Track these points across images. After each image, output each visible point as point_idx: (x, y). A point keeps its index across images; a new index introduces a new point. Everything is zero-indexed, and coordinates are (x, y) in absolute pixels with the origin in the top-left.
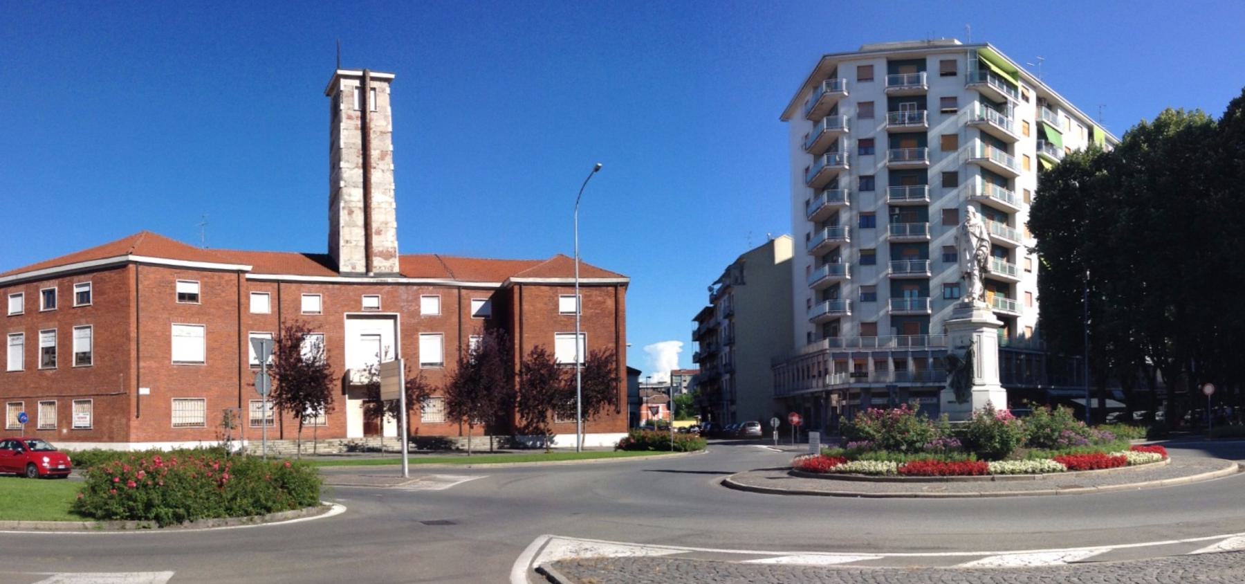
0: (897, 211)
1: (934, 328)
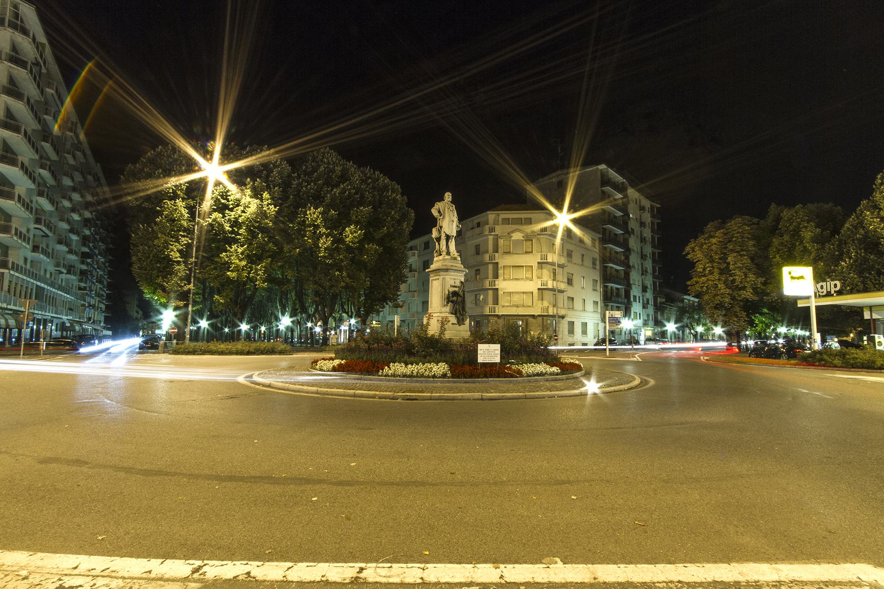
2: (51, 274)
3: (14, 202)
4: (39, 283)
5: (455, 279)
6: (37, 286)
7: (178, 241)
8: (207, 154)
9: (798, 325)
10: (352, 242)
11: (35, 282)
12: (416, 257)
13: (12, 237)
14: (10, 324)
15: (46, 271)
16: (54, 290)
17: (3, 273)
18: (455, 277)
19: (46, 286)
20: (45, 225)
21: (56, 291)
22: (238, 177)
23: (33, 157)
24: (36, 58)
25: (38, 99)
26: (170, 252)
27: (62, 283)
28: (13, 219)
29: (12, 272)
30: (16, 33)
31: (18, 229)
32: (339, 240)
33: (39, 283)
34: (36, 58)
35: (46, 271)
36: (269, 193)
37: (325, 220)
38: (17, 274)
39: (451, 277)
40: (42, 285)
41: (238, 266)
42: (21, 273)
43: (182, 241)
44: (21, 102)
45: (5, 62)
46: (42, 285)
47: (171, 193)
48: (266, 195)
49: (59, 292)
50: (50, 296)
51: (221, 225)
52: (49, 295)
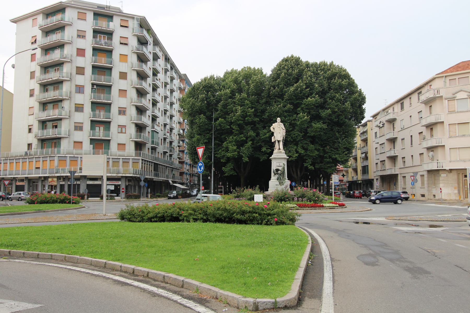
0: (95, 87)
1: (113, 147)
5: (279, 163)
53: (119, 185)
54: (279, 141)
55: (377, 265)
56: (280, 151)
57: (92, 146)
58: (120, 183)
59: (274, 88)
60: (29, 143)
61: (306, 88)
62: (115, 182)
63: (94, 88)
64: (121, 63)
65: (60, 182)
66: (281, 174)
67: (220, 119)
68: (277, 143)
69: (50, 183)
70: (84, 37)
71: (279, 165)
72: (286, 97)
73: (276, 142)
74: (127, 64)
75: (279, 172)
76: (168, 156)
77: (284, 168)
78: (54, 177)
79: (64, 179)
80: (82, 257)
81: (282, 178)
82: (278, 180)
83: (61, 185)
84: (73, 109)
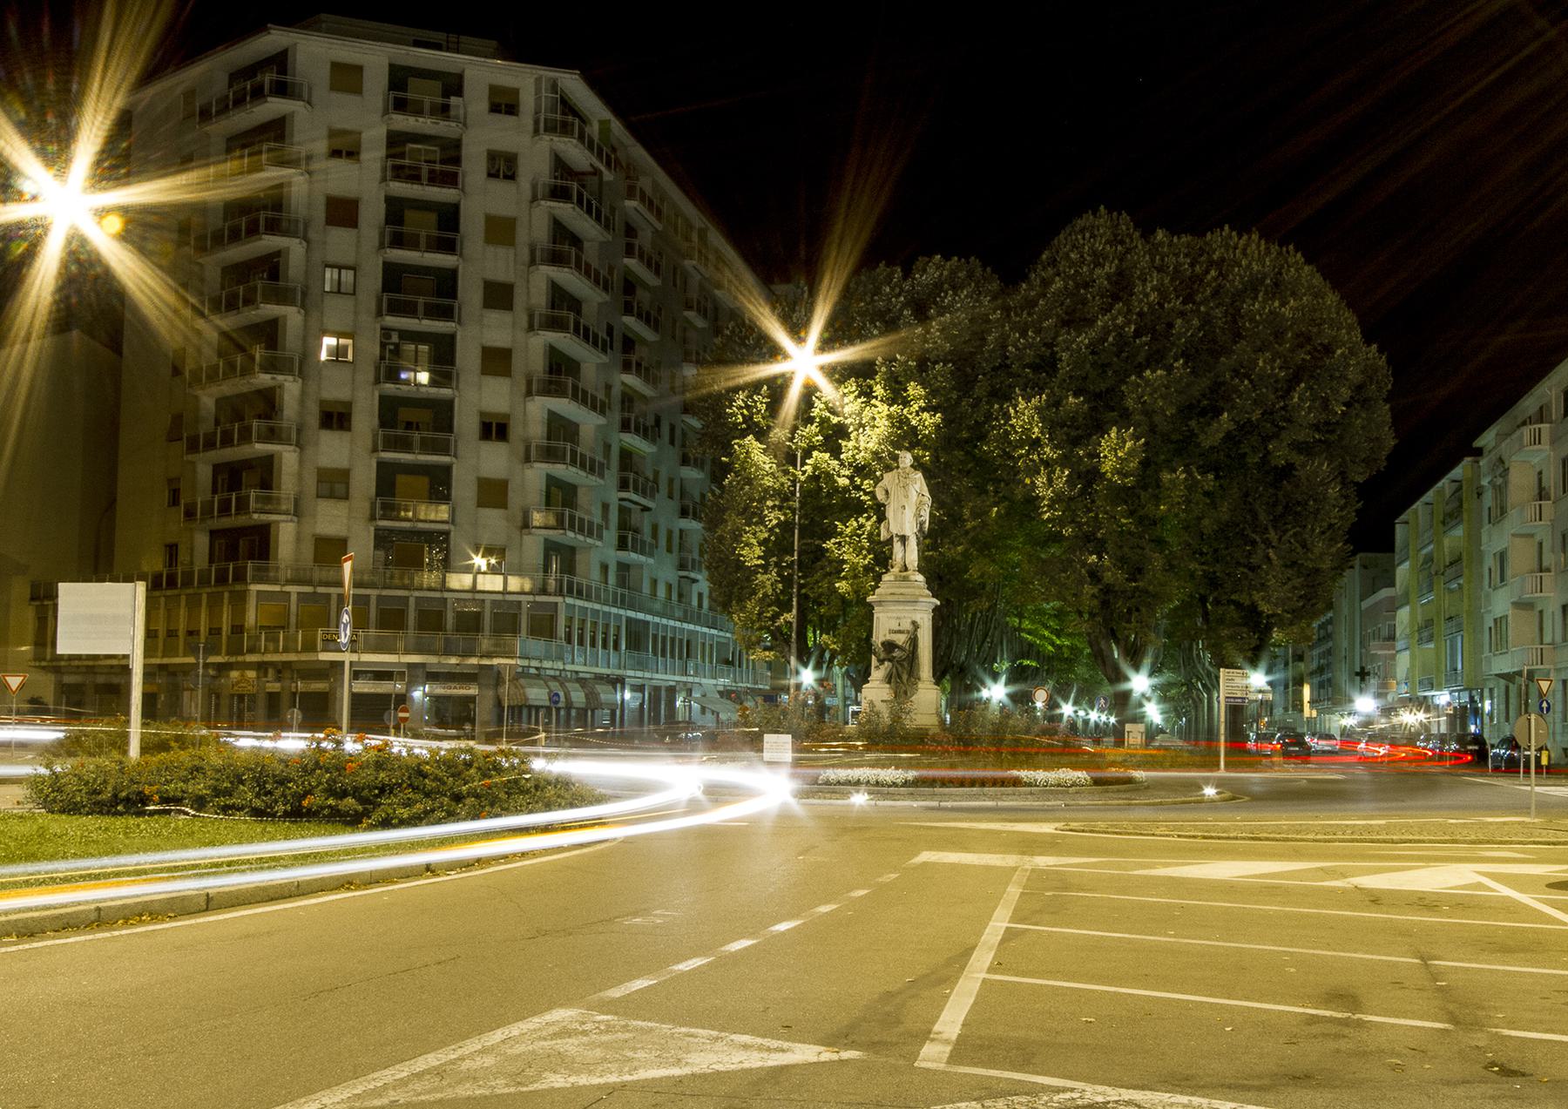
2: (669, 587)
3: (564, 466)
4: (631, 614)
5: (898, 618)
6: (629, 620)
7: (762, 521)
8: (797, 329)
9: (972, 701)
10: (1119, 472)
11: (622, 612)
12: (1545, 445)
13: (565, 534)
14: (574, 699)
15: (654, 582)
16: (671, 623)
17: (557, 603)
18: (899, 615)
19: (649, 618)
20: (636, 490)
21: (678, 624)
22: (839, 374)
23: (599, 361)
24: (591, 165)
25: (602, 239)
26: (743, 549)
27: (700, 605)
28: (581, 492)
29: (569, 600)
30: (555, 139)
31: (584, 520)
32: (1088, 476)
33: (631, 614)
34: (591, 165)
35: (654, 582)
36: (923, 384)
37: (1052, 425)
38: (579, 603)
39: (889, 615)
40: (641, 616)
41: (854, 567)
42: (588, 598)
43: (771, 521)
44: (566, 270)
45: (543, 202)
46: (641, 616)
47: (741, 424)
48: (914, 389)
49: (685, 625)
50: (664, 638)
51: (829, 477)
52: (678, 636)
53: (472, 699)
54: (903, 539)
55: (1344, 1036)
56: (905, 574)
57: (381, 553)
58: (472, 691)
59: (1024, 334)
60: (170, 540)
61: (1137, 334)
62: (455, 688)
63: (392, 344)
64: (491, 249)
65: (268, 684)
66: (904, 660)
67: (815, 453)
68: (897, 546)
69: (236, 688)
70: (352, 154)
71: (897, 628)
72: (1064, 367)
73: (895, 539)
74: (511, 251)
75: (897, 653)
76: (1490, 628)
77: (914, 641)
78: (250, 666)
79: (279, 672)
80: (1346, 1015)
81: (905, 677)
82: (889, 682)
83: (270, 694)
84: (313, 420)
